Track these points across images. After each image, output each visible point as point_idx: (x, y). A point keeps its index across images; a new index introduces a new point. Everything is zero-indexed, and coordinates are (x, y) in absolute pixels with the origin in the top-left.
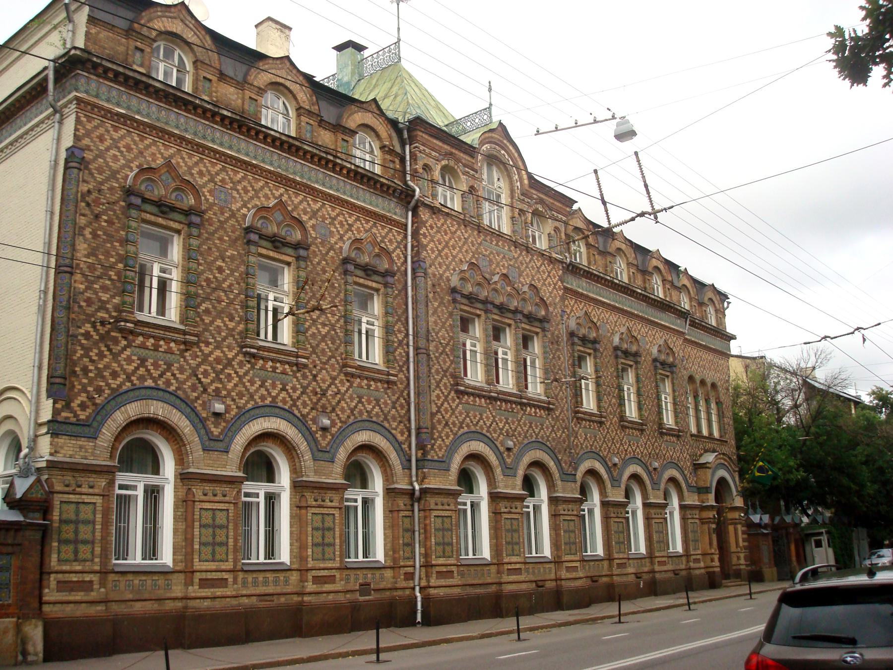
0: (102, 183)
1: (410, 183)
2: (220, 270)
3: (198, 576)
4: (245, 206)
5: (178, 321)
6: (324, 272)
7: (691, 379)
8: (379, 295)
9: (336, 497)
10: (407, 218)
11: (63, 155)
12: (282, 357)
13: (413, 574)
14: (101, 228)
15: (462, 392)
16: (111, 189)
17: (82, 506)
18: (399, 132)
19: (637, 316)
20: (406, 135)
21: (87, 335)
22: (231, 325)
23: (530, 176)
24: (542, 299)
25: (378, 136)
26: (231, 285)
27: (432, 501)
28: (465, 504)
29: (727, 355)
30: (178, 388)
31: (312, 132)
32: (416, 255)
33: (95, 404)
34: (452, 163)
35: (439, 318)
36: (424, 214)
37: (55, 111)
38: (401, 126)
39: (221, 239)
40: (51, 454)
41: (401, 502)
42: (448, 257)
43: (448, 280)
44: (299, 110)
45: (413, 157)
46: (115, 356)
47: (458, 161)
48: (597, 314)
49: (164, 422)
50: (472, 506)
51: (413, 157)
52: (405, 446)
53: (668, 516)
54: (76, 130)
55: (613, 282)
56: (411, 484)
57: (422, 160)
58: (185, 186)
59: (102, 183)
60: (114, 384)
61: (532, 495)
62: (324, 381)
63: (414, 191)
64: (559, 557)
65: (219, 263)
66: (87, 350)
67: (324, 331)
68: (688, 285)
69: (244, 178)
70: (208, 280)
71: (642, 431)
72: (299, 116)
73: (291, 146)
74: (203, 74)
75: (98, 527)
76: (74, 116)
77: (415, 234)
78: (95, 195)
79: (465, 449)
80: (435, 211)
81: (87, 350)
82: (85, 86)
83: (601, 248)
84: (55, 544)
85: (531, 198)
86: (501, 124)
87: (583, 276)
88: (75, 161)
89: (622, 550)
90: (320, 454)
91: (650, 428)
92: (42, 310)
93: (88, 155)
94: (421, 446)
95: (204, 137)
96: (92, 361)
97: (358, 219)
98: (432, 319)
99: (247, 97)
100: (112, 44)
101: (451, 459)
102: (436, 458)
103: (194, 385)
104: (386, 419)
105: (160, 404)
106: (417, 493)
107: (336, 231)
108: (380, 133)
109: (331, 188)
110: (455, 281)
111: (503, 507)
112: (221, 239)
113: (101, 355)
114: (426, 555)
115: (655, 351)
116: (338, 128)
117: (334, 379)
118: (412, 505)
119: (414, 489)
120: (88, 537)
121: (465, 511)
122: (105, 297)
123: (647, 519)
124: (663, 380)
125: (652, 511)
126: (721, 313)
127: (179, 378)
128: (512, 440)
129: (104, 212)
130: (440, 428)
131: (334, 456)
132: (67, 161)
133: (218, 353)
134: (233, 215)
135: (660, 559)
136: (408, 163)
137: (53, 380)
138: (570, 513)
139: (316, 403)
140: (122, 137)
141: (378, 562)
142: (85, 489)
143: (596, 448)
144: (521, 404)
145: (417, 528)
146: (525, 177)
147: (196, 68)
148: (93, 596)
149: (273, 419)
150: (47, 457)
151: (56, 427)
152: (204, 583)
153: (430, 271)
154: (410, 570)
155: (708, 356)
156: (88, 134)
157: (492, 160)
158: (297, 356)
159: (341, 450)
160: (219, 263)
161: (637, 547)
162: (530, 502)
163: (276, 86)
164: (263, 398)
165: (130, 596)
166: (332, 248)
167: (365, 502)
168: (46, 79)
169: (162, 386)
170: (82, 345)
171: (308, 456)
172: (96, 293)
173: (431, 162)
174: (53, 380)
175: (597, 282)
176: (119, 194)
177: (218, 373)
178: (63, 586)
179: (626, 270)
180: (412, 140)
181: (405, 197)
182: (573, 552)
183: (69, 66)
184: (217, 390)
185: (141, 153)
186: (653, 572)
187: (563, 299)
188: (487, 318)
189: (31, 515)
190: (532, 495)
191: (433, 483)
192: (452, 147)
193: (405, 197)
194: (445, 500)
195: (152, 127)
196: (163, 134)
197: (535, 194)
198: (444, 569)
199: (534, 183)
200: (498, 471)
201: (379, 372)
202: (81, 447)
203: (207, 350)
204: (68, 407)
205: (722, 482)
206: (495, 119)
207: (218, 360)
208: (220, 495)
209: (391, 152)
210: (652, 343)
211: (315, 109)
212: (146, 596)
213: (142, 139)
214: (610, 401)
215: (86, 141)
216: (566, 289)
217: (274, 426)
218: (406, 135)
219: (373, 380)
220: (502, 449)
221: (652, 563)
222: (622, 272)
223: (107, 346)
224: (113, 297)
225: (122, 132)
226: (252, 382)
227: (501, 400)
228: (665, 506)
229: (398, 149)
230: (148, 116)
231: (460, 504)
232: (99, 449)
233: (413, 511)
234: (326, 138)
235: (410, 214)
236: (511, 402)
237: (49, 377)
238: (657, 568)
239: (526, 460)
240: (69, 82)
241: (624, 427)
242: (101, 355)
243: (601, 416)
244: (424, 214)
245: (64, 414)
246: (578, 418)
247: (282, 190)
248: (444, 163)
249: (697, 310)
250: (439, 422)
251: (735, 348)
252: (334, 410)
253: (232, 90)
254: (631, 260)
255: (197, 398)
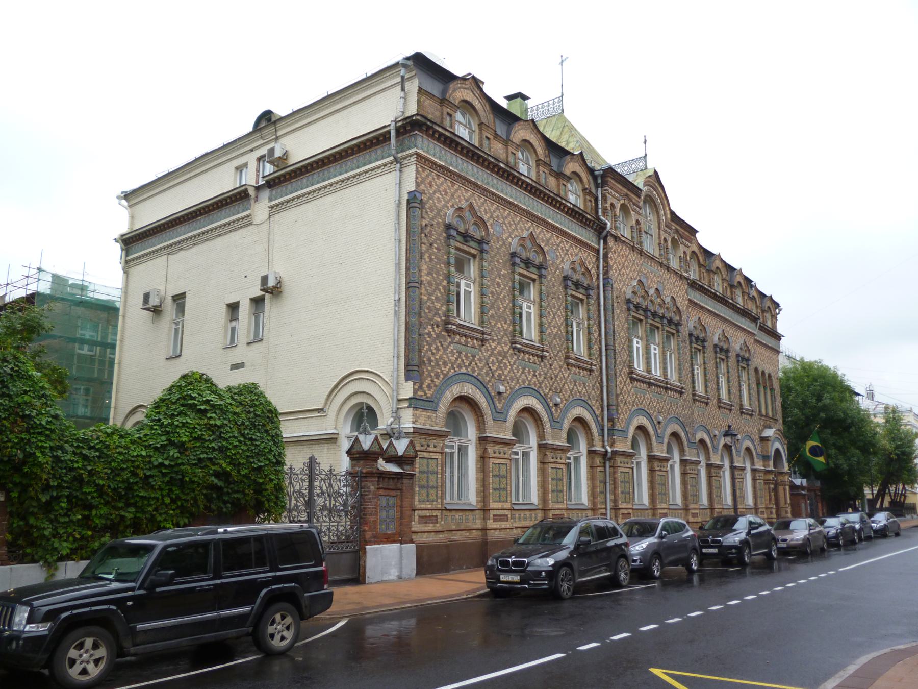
0: (432, 219)
1: (602, 218)
2: (498, 284)
3: (492, 513)
4: (510, 236)
5: (477, 323)
6: (554, 286)
7: (756, 370)
8: (583, 304)
9: (563, 456)
10: (599, 245)
11: (405, 197)
12: (534, 351)
13: (606, 514)
14: (434, 253)
15: (633, 377)
16: (438, 223)
17: (430, 461)
18: (595, 178)
19: (727, 320)
20: (599, 181)
21: (429, 334)
22: (506, 326)
23: (673, 213)
24: (678, 308)
25: (581, 180)
26: (505, 296)
27: (619, 460)
28: (517, 454)
29: (778, 352)
30: (479, 374)
31: (546, 178)
32: (606, 273)
33: (435, 386)
34: (627, 202)
35: (620, 320)
36: (611, 242)
37: (396, 160)
38: (596, 173)
39: (498, 261)
40: (414, 423)
41: (598, 461)
42: (626, 274)
43: (625, 293)
44: (538, 161)
45: (604, 196)
46: (445, 349)
47: (630, 200)
48: (542, 235)
49: (472, 399)
50: (459, 450)
51: (604, 198)
52: (600, 419)
53: (635, 465)
54: (417, 178)
55: (715, 294)
56: (604, 447)
57: (610, 200)
58: (481, 222)
59: (432, 219)
60: (445, 370)
61: (457, 433)
62: (556, 369)
63: (606, 224)
64: (687, 506)
65: (498, 280)
66: (430, 345)
67: (555, 331)
68: (756, 296)
69: (509, 214)
70: (492, 293)
71: (730, 410)
72: (538, 166)
73: (474, 154)
74: (485, 134)
75: (439, 476)
76: (414, 167)
77: (606, 256)
78: (429, 228)
79: (456, 390)
80: (616, 238)
81: (430, 345)
82: (423, 145)
83: (555, 168)
84: (417, 489)
85: (671, 229)
86: (656, 172)
87: (697, 289)
88: (415, 202)
89: (627, 500)
90: (498, 415)
91: (736, 408)
92: (397, 314)
93: (424, 198)
94: (611, 420)
95: (488, 184)
96: (433, 354)
97: (571, 246)
98: (616, 323)
99: (445, 113)
100: (433, 111)
101: (628, 429)
102: (424, 397)
103: (487, 372)
104: (589, 398)
105: (470, 386)
106: (609, 455)
107: (563, 257)
108: (532, 141)
109: (502, 192)
110: (629, 295)
111: (656, 465)
112: (498, 261)
113: (437, 349)
114: (615, 501)
115: (566, 266)
116: (559, 175)
117: (561, 367)
118: (605, 463)
119: (607, 451)
120: (434, 483)
121: (452, 454)
122: (438, 305)
123: (684, 474)
124: (696, 353)
125: (656, 464)
126: (774, 317)
127: (480, 370)
128: (503, 385)
129: (435, 242)
130: (622, 405)
131: (437, 405)
132: (408, 202)
133: (499, 348)
134: (504, 243)
135: (496, 512)
136: (600, 202)
137: (410, 368)
138: (502, 455)
139: (552, 386)
140: (442, 184)
141: (469, 504)
142: (431, 449)
143: (535, 385)
144: (666, 389)
145: (608, 480)
146: (668, 212)
147: (481, 130)
148: (438, 527)
149: (529, 397)
150: (411, 425)
151: (414, 402)
152: (498, 518)
153: (614, 286)
154: (603, 511)
155: (767, 353)
156: (423, 182)
157: (649, 200)
158: (543, 351)
159: (566, 421)
160: (498, 280)
161: (579, 496)
162: (519, 448)
163: (467, 106)
164: (524, 382)
165: (454, 527)
166: (557, 268)
167: (460, 449)
168: (389, 132)
169: (470, 373)
170: (427, 342)
171: (548, 426)
172: (433, 303)
173: (615, 201)
174: (410, 368)
175: (705, 294)
176: (442, 228)
177: (500, 362)
178: (424, 520)
179: (477, 131)
180: (604, 183)
181: (599, 229)
182: (502, 499)
183: (409, 127)
184: (499, 375)
185: (452, 195)
186: (484, 530)
187: (688, 307)
188: (647, 322)
189: (406, 467)
190: (457, 433)
191: (619, 447)
192: (629, 190)
193: (599, 229)
194: (626, 460)
195: (459, 176)
196: (465, 181)
197: (674, 226)
198: (427, 513)
199: (675, 217)
200: (654, 439)
201: (534, 347)
202: (429, 417)
203: (493, 345)
204: (421, 387)
205: (777, 451)
206: (650, 166)
207: (499, 353)
208: (432, 446)
209: (590, 193)
210: (737, 342)
211: (547, 160)
212: (462, 527)
213: (453, 184)
214: (712, 385)
215: (422, 187)
216: (690, 300)
217: (530, 402)
218: (599, 181)
219: (533, 355)
220: (656, 422)
221: (485, 519)
222: (718, 287)
223: (440, 342)
224: (442, 305)
225: (442, 179)
226: (518, 370)
227: (655, 385)
228: (666, 460)
229: (593, 191)
230: (456, 167)
231: (447, 446)
232: (436, 421)
233: (605, 467)
234: (552, 182)
235: (602, 242)
236: (660, 387)
237: (407, 365)
238: (491, 524)
239: (450, 395)
240: (406, 139)
241: (720, 407)
242: (437, 349)
243: (708, 399)
244: (611, 242)
245: (419, 393)
246: (514, 349)
247: (530, 224)
248: (622, 202)
249: (759, 312)
250: (621, 401)
251: (784, 344)
252: (561, 391)
253: (500, 145)
254: (724, 277)
255: (489, 381)
